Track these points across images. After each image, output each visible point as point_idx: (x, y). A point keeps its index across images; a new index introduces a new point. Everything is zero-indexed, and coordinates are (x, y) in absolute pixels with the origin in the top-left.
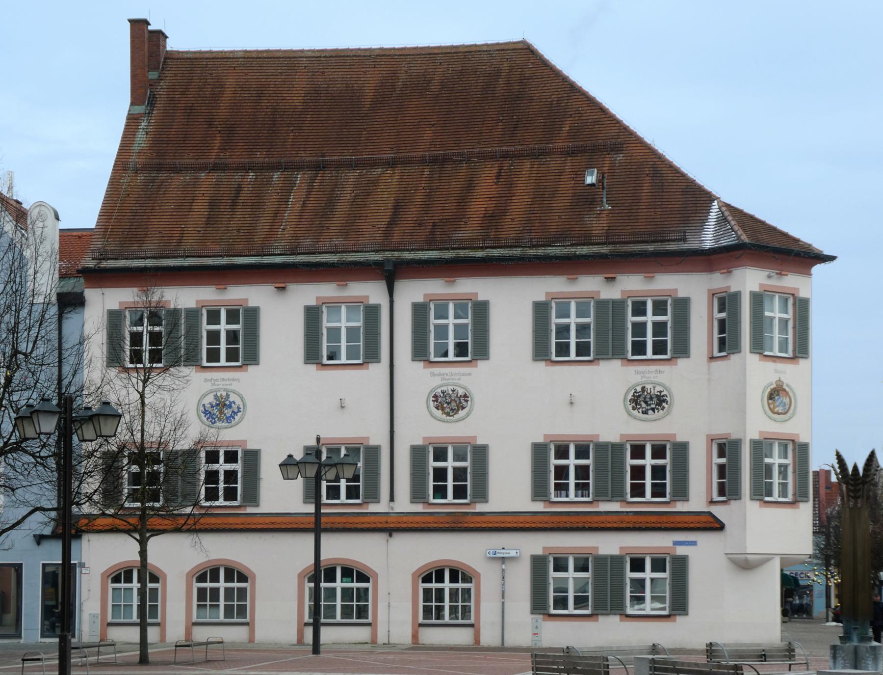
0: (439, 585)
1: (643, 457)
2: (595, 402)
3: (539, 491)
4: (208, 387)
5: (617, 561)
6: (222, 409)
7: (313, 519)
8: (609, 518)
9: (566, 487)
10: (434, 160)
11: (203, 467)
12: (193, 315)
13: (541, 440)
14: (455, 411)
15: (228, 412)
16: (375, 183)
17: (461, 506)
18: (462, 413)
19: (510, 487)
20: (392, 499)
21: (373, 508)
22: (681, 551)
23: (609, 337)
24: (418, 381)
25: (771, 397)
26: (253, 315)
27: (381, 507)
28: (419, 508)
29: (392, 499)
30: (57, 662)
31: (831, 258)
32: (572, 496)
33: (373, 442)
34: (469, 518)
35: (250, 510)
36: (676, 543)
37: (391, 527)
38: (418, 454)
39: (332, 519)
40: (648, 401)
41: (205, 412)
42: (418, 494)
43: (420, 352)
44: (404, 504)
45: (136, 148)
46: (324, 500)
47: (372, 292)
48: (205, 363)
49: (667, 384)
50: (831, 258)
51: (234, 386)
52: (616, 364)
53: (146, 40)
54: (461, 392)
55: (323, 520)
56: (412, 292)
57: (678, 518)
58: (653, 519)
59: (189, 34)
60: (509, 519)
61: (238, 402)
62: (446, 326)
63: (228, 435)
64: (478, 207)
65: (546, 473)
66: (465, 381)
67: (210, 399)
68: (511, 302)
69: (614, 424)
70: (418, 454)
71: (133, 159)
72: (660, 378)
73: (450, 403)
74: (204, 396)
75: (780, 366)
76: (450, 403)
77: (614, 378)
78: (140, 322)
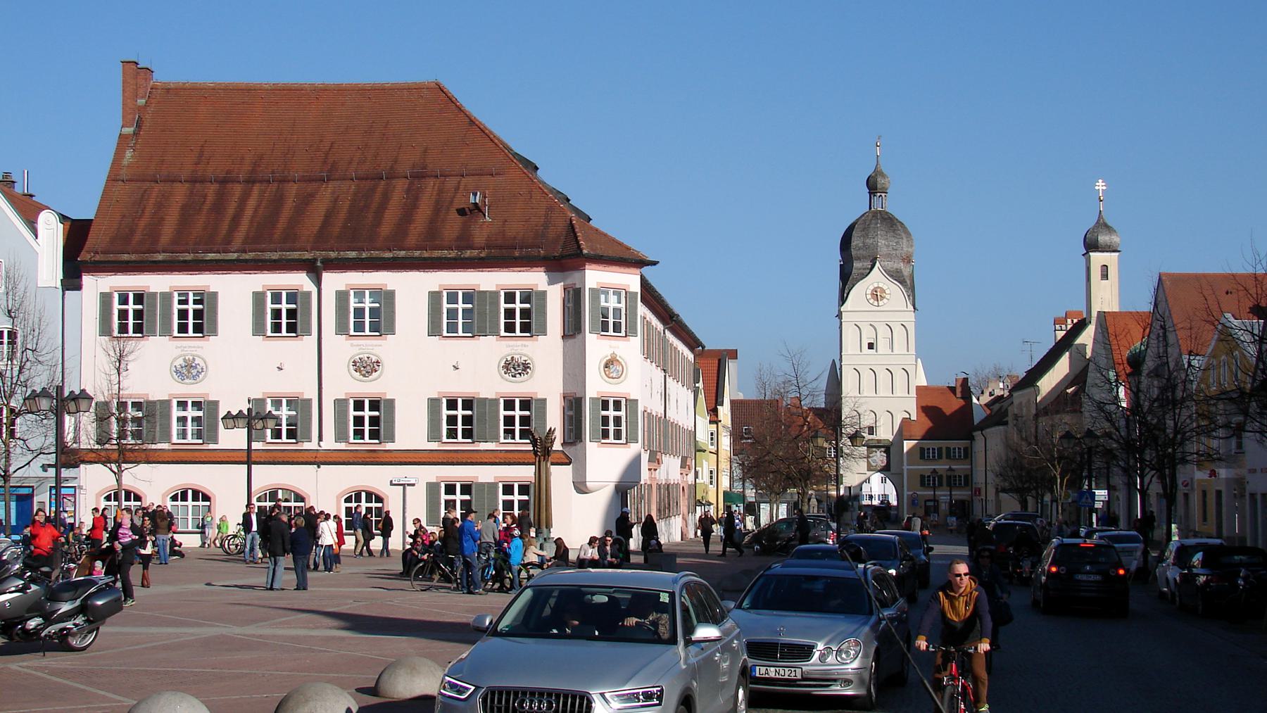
0: (369, 505)
1: (363, 410)
2: (478, 367)
3: (434, 435)
4: (178, 352)
5: (493, 486)
6: (188, 370)
7: (245, 454)
8: (398, 454)
9: (513, 432)
10: (203, 181)
12: (167, 297)
13: (436, 396)
14: (370, 373)
15: (194, 372)
16: (312, 195)
17: (372, 445)
18: (375, 375)
19: (410, 431)
20: (320, 438)
21: (306, 446)
23: (477, 317)
24: (340, 350)
25: (606, 366)
26: (390, 295)
27: (313, 445)
28: (342, 446)
29: (320, 438)
30: (1249, 544)
31: (654, 263)
32: (367, 439)
34: (380, 454)
35: (212, 446)
37: (319, 459)
38: (340, 404)
40: (517, 368)
41: (176, 372)
42: (341, 435)
43: (341, 328)
44: (329, 443)
45: (125, 162)
47: (300, 280)
48: (503, 333)
50: (654, 263)
53: (135, 72)
56: (334, 281)
57: (166, 455)
58: (520, 455)
59: (167, 73)
61: (202, 364)
62: (514, 310)
64: (391, 216)
65: (440, 421)
66: (377, 351)
67: (180, 362)
68: (412, 289)
70: (340, 404)
71: (124, 173)
72: (525, 351)
73: (366, 367)
74: (176, 359)
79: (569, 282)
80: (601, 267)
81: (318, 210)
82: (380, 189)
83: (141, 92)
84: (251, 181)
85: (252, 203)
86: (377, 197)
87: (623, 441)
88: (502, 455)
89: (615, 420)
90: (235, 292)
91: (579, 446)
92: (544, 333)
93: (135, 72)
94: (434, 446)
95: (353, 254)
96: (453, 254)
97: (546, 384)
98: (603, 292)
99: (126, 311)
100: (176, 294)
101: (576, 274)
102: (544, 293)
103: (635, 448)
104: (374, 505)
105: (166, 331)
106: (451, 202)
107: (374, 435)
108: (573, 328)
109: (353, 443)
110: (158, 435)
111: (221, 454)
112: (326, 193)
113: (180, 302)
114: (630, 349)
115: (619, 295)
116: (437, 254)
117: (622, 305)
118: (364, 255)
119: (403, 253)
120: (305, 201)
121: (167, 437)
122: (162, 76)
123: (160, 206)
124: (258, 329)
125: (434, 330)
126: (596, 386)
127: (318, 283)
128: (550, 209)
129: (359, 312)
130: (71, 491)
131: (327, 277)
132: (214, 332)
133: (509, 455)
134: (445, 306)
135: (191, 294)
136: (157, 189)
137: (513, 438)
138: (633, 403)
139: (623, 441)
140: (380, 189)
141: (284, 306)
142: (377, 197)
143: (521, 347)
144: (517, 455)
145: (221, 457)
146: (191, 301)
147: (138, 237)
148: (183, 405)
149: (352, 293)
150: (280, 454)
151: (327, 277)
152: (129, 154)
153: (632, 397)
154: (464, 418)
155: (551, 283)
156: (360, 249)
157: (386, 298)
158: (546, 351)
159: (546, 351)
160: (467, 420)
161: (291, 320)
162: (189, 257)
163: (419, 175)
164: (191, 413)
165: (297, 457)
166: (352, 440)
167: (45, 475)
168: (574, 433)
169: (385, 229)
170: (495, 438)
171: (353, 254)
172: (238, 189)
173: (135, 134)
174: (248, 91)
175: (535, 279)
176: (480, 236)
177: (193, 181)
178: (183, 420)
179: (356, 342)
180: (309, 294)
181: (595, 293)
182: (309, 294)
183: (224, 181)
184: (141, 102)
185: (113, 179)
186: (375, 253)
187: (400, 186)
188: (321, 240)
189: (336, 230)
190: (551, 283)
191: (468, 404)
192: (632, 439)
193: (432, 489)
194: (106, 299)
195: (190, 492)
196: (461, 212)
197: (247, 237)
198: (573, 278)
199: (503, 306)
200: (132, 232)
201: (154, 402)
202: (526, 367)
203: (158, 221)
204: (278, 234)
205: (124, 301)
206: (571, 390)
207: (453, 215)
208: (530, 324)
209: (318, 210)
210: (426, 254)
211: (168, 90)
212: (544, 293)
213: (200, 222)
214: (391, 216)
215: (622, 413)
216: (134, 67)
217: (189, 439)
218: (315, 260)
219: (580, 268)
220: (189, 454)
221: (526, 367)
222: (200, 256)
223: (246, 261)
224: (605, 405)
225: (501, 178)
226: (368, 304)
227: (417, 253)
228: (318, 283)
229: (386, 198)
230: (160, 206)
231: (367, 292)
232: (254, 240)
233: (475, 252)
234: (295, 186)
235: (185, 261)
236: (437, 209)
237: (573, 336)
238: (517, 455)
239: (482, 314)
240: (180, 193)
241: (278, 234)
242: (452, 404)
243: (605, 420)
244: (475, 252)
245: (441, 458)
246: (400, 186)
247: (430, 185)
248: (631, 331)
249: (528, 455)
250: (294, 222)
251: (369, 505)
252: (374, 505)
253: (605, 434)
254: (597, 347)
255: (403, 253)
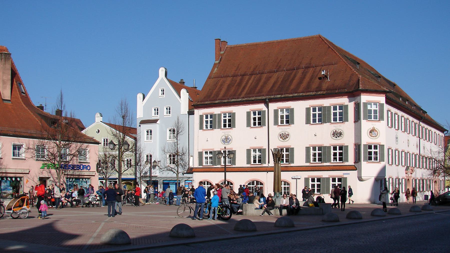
0: (285, 186)
2: (323, 135)
3: (308, 160)
4: (223, 134)
5: (328, 179)
6: (226, 140)
11: (332, 151)
12: (220, 115)
13: (308, 146)
14: (285, 139)
15: (228, 140)
16: (270, 77)
19: (299, 159)
20: (269, 163)
21: (264, 165)
22: (345, 176)
23: (323, 116)
24: (276, 131)
25: (371, 132)
29: (269, 163)
32: (338, 161)
33: (264, 148)
35: (234, 166)
36: (344, 174)
39: (229, 169)
43: (276, 123)
45: (214, 72)
46: (227, 164)
47: (261, 107)
49: (342, 129)
51: (230, 134)
52: (328, 124)
53: (220, 44)
54: (287, 133)
55: (227, 169)
56: (273, 106)
57: (219, 169)
60: (299, 168)
61: (231, 138)
63: (229, 147)
64: (295, 82)
66: (288, 130)
67: (224, 137)
68: (300, 107)
69: (219, 147)
73: (337, 134)
75: (374, 123)
76: (284, 137)
77: (327, 128)
78: (226, 117)
79: (356, 101)
80: (368, 94)
81: (272, 81)
82: (293, 73)
83: (222, 49)
84: (251, 75)
85: (250, 82)
86: (292, 76)
87: (378, 161)
88: (332, 167)
89: (373, 153)
90: (241, 112)
91: (359, 163)
92: (347, 120)
93: (220, 44)
94: (308, 164)
95: (279, 96)
96: (314, 93)
97: (348, 140)
98: (369, 104)
99: (208, 121)
100: (223, 114)
101: (358, 98)
102: (347, 105)
103: (382, 164)
104: (286, 186)
105: (219, 127)
106: (317, 75)
107: (341, 159)
108: (357, 119)
109: (312, 163)
110: (217, 162)
111: (348, 167)
112: (275, 76)
113: (224, 117)
114: (381, 126)
115: (376, 105)
116: (308, 94)
117: (378, 109)
118: (283, 96)
119: (296, 94)
120: (268, 79)
121: (329, 161)
122: (231, 43)
123: (221, 85)
124: (248, 125)
125: (308, 122)
126: (366, 140)
127: (268, 107)
128: (352, 75)
129: (282, 117)
130: (191, 182)
131: (270, 105)
132: (234, 126)
133: (334, 167)
134: (312, 113)
135: (227, 114)
136: (222, 80)
137: (336, 161)
138: (382, 147)
139: (378, 161)
140: (293, 73)
141: (257, 116)
142: (292, 76)
143: (340, 127)
144: (337, 167)
145: (236, 170)
146: (227, 116)
147: (213, 96)
148: (206, 153)
149: (279, 110)
150: (255, 168)
151: (270, 105)
152: (216, 69)
153: (382, 144)
154: (322, 153)
155: (350, 101)
156: (282, 94)
157: (291, 111)
158: (348, 128)
159: (348, 128)
160: (320, 155)
161: (260, 121)
162: (226, 101)
163: (307, 68)
164: (209, 155)
165: (261, 169)
166: (332, 161)
167: (183, 176)
168: (357, 160)
169: (292, 87)
170: (329, 161)
171: (279, 96)
172: (247, 77)
173: (219, 63)
174: (256, 45)
175: (344, 100)
176: (325, 86)
177: (233, 76)
178: (206, 158)
179: (281, 127)
180: (265, 111)
181: (365, 104)
182: (265, 111)
183: (243, 75)
184: (222, 52)
185: (209, 78)
186: (287, 95)
187: (301, 71)
188: (270, 92)
189: (276, 88)
190: (350, 101)
191: (320, 149)
192: (382, 160)
193: (306, 180)
194: (201, 117)
195: (255, 182)
196: (320, 78)
197: (246, 93)
198: (357, 99)
199: (332, 111)
200: (211, 94)
201: (216, 151)
202: (334, 134)
203: (220, 90)
204: (257, 91)
205: (207, 117)
206: (357, 142)
207: (317, 80)
208: (343, 118)
209: (272, 81)
210: (304, 94)
211: (231, 48)
212: (347, 105)
213: (233, 89)
214: (295, 82)
215: (378, 150)
216: (219, 41)
217: (209, 164)
218: (266, 99)
219: (359, 95)
220: (208, 169)
221: (341, 134)
222: (229, 100)
223: (243, 101)
224: (370, 147)
225: (336, 65)
226: (285, 114)
227: (301, 94)
228: (268, 107)
229: (295, 76)
230: (221, 85)
231: (285, 110)
232: (249, 94)
233: (322, 92)
234: (265, 75)
235: (224, 103)
236: (312, 78)
237: (357, 121)
238: (337, 167)
239: (325, 115)
240: (229, 80)
241: (257, 91)
242: (314, 149)
243: (370, 153)
244: (322, 92)
245: (309, 169)
246: (301, 71)
247: (311, 70)
248: (382, 118)
249: (352, 167)
250: (263, 87)
251: (285, 186)
252: (286, 186)
253: (370, 158)
254: (366, 125)
255: (296, 94)
